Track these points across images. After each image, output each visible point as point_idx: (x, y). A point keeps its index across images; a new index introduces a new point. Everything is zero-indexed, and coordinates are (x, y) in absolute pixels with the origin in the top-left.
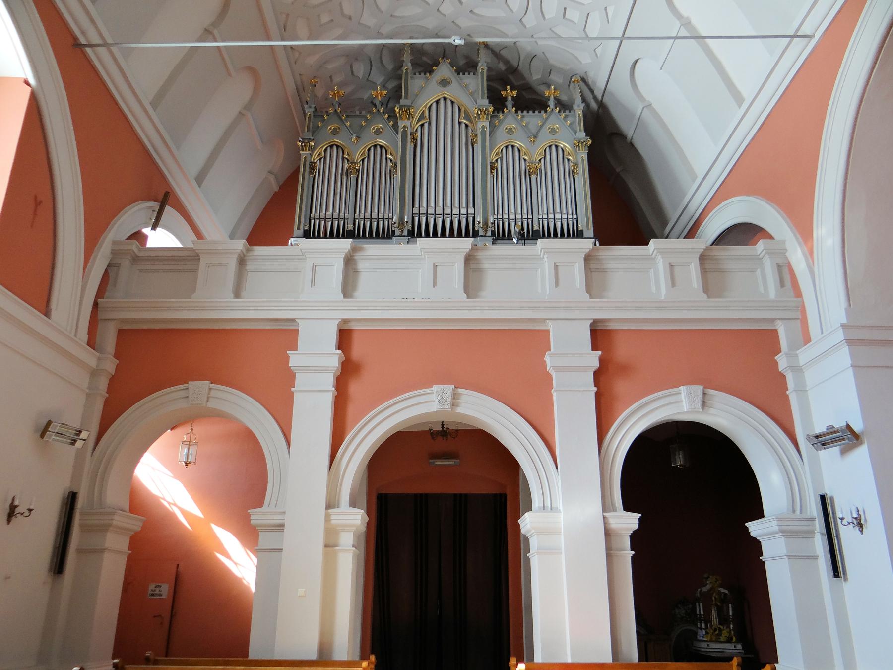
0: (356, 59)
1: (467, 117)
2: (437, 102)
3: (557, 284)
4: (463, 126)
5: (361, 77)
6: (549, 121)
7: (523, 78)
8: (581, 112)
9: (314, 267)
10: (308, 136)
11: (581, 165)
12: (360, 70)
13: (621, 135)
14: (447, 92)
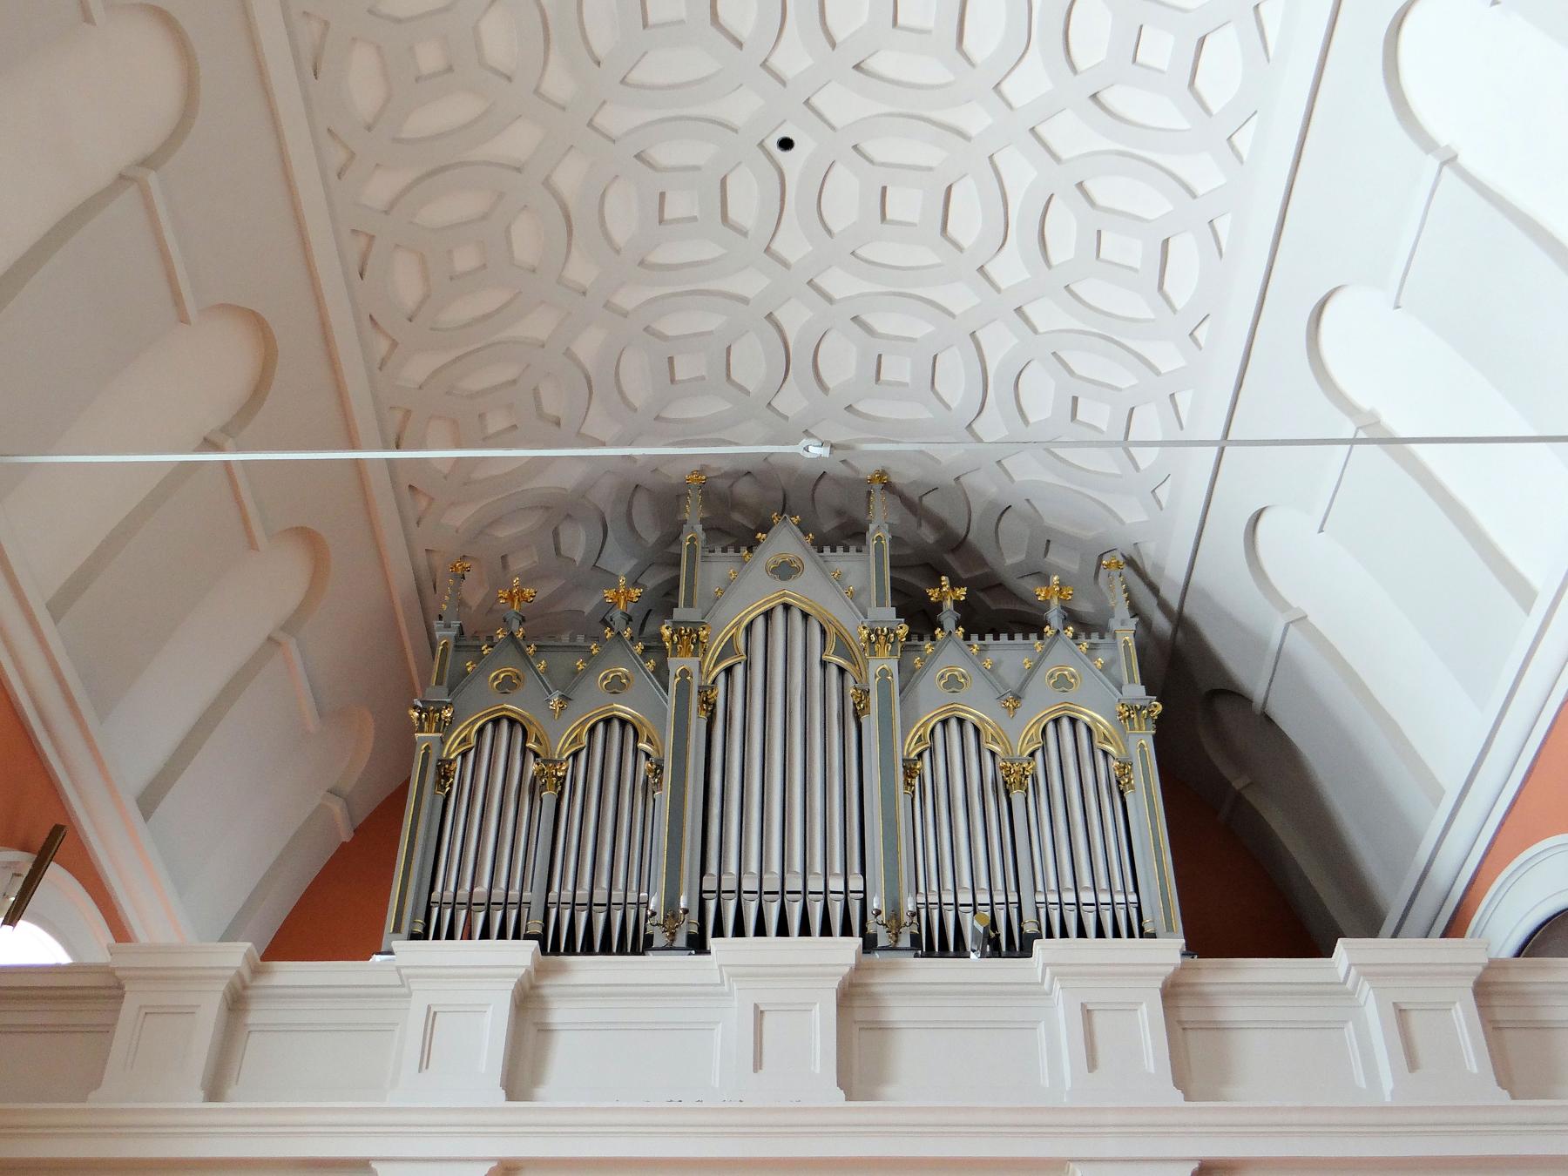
0: (569, 516)
1: (844, 649)
2: (768, 615)
3: (1092, 1064)
4: (834, 671)
5: (578, 558)
6: (1049, 660)
7: (981, 561)
8: (1129, 638)
9: (431, 1016)
10: (439, 694)
11: (1138, 766)
12: (577, 542)
13: (1233, 695)
14: (797, 591)
